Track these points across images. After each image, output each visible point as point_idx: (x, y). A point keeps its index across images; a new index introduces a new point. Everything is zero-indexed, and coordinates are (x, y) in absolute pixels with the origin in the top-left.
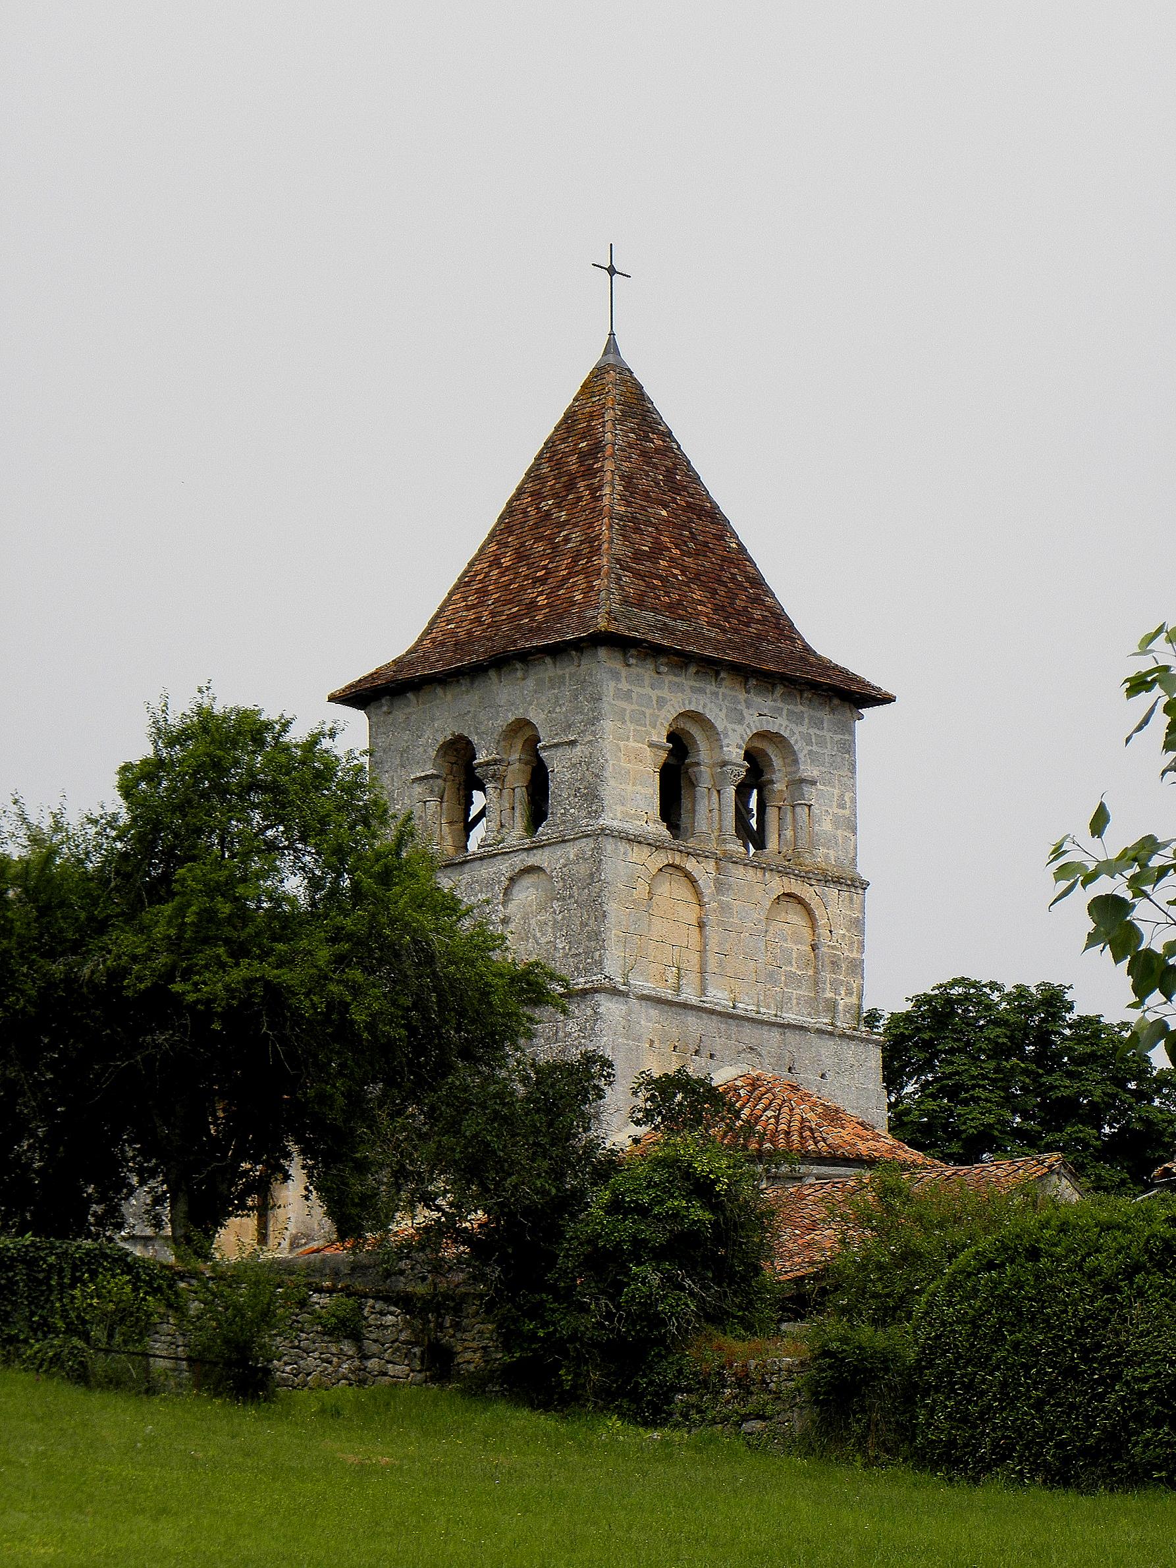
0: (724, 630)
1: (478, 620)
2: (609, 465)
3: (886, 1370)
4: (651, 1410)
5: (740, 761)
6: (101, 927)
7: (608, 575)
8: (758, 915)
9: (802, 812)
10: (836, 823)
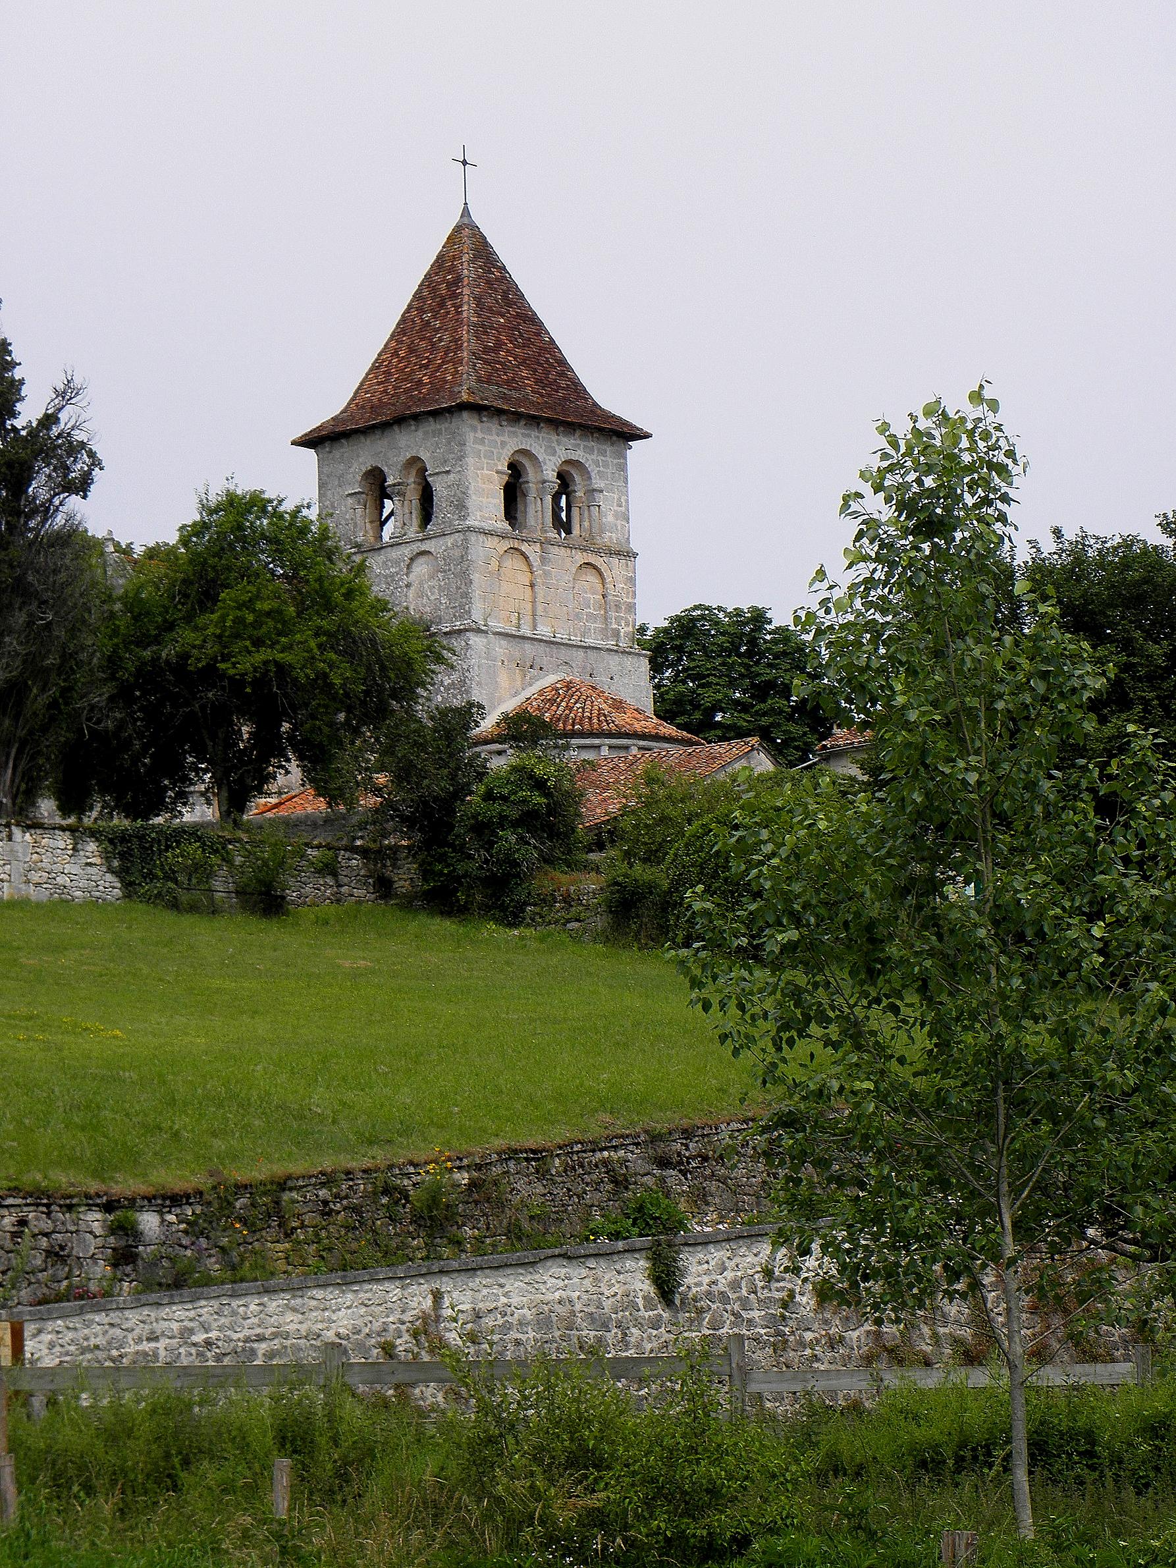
0: (542, 396)
1: (385, 391)
2: (466, 291)
3: (651, 893)
4: (512, 917)
5: (555, 480)
6: (170, 626)
7: (467, 363)
8: (568, 577)
9: (595, 510)
10: (616, 516)
